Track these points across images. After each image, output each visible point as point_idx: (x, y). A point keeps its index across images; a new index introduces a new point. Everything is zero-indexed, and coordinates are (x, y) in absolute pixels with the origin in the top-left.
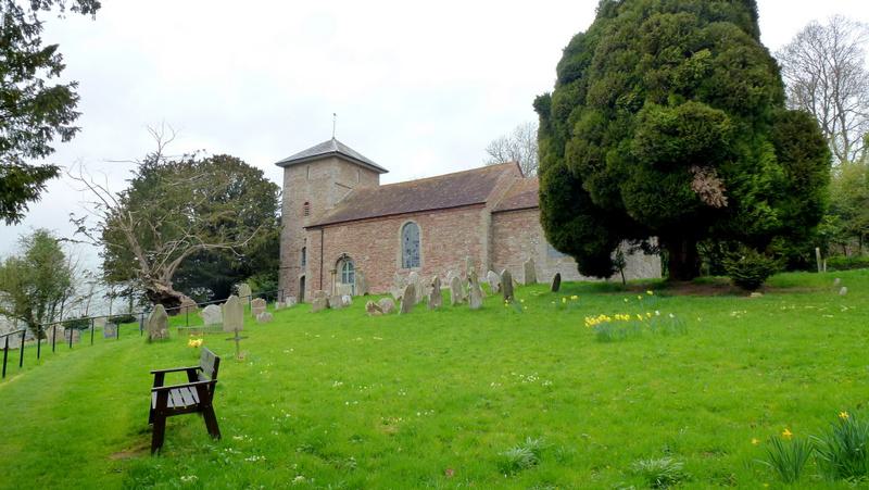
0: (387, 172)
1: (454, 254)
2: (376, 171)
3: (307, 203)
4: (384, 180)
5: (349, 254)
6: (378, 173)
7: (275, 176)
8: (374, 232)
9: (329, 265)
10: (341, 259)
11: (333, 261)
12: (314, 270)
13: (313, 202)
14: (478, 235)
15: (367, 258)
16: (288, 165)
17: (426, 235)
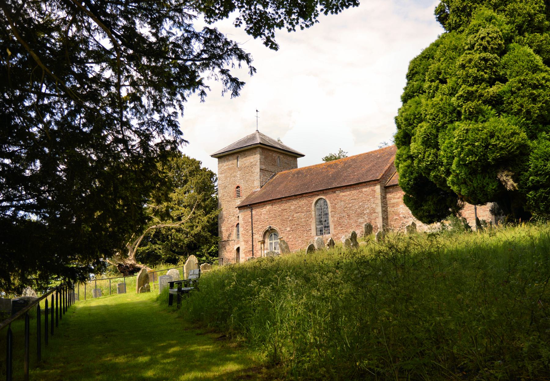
0: (303, 156)
1: (356, 222)
2: (296, 155)
3: (238, 187)
4: (301, 163)
5: (274, 227)
6: (297, 157)
7: (210, 164)
8: (293, 207)
9: (258, 237)
10: (267, 231)
11: (262, 233)
12: (246, 242)
13: (242, 186)
14: (374, 206)
15: (288, 229)
16: (222, 157)
17: (334, 207)
